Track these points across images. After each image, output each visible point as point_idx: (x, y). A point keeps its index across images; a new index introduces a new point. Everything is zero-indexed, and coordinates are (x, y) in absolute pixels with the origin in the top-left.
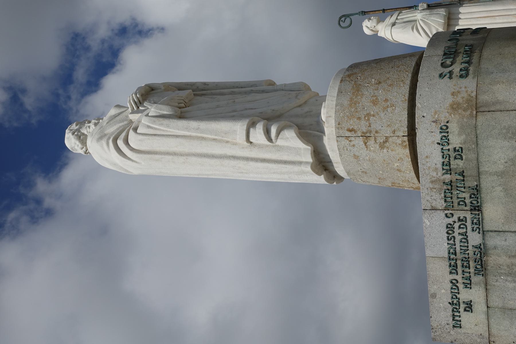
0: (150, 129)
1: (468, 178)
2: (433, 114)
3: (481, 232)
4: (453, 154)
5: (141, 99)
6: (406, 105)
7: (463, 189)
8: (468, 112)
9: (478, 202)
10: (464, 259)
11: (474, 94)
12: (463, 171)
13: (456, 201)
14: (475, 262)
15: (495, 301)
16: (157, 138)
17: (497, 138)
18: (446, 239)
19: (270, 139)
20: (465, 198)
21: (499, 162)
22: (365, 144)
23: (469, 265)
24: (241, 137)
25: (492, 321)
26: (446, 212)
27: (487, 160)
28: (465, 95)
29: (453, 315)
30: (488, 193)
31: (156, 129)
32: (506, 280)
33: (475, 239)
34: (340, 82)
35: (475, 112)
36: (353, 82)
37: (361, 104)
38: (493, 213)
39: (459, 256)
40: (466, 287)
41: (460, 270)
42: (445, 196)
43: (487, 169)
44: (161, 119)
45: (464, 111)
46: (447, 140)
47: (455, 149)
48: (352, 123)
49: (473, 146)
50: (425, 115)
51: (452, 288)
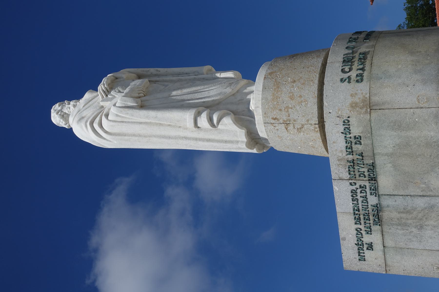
0: (118, 118)
1: (366, 158)
2: (337, 111)
3: (377, 195)
4: (354, 141)
5: (108, 89)
6: (316, 100)
7: (362, 166)
8: (364, 110)
9: (374, 175)
10: (365, 214)
11: (367, 96)
12: (362, 153)
13: (357, 174)
14: (374, 216)
15: (389, 243)
16: (124, 124)
17: (386, 130)
18: (351, 200)
19: (213, 125)
20: (364, 172)
21: (388, 146)
22: (286, 129)
23: (369, 218)
24: (190, 123)
25: (387, 256)
26: (351, 181)
27: (379, 145)
28: (361, 97)
29: (359, 252)
30: (381, 168)
31: (123, 117)
32: (397, 229)
33: (372, 200)
34: (264, 79)
35: (369, 110)
36: (274, 80)
37: (281, 99)
38: (385, 182)
39: (362, 212)
40: (368, 233)
41: (362, 221)
42: (349, 170)
43: (380, 151)
44: (126, 109)
45: (361, 109)
46: (348, 131)
47: (355, 137)
48: (276, 113)
49: (369, 135)
50: (331, 111)
51: (357, 234)
